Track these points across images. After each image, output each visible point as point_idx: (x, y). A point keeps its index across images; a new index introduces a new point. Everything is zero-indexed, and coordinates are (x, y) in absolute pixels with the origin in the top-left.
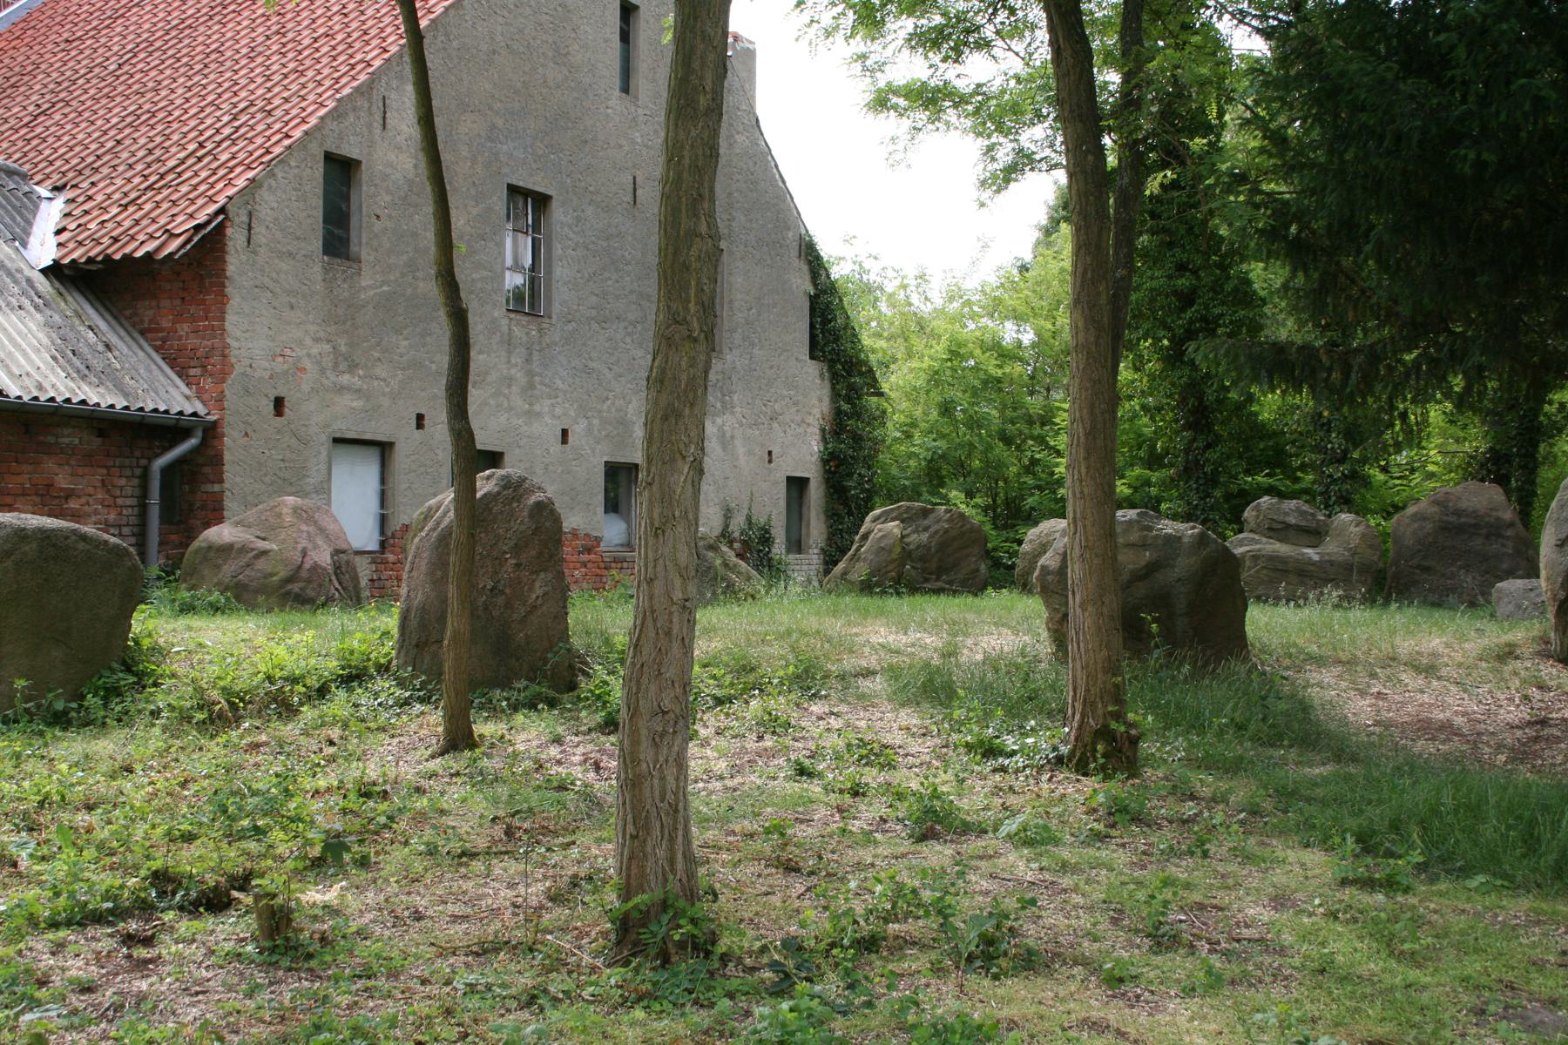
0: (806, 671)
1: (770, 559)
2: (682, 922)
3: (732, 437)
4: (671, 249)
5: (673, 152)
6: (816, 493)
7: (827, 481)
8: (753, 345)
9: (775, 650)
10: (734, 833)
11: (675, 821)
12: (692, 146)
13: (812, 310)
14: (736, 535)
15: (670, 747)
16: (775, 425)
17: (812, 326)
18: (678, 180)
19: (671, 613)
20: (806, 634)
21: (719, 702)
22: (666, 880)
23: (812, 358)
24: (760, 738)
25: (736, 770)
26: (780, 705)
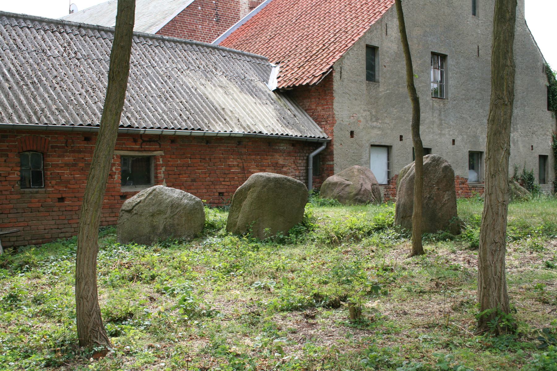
0: (549, 228)
1: (533, 186)
2: (504, 320)
3: (517, 141)
4: (496, 72)
5: (496, 35)
6: (550, 161)
8: (525, 106)
9: (537, 220)
10: (522, 288)
11: (500, 282)
12: (504, 33)
13: (548, 91)
14: (519, 177)
15: (498, 256)
16: (534, 136)
17: (548, 98)
18: (499, 46)
19: (498, 206)
20: (549, 214)
21: (515, 239)
22: (497, 304)
23: (548, 110)
24: (531, 253)
25: (522, 265)
26: (539, 241)
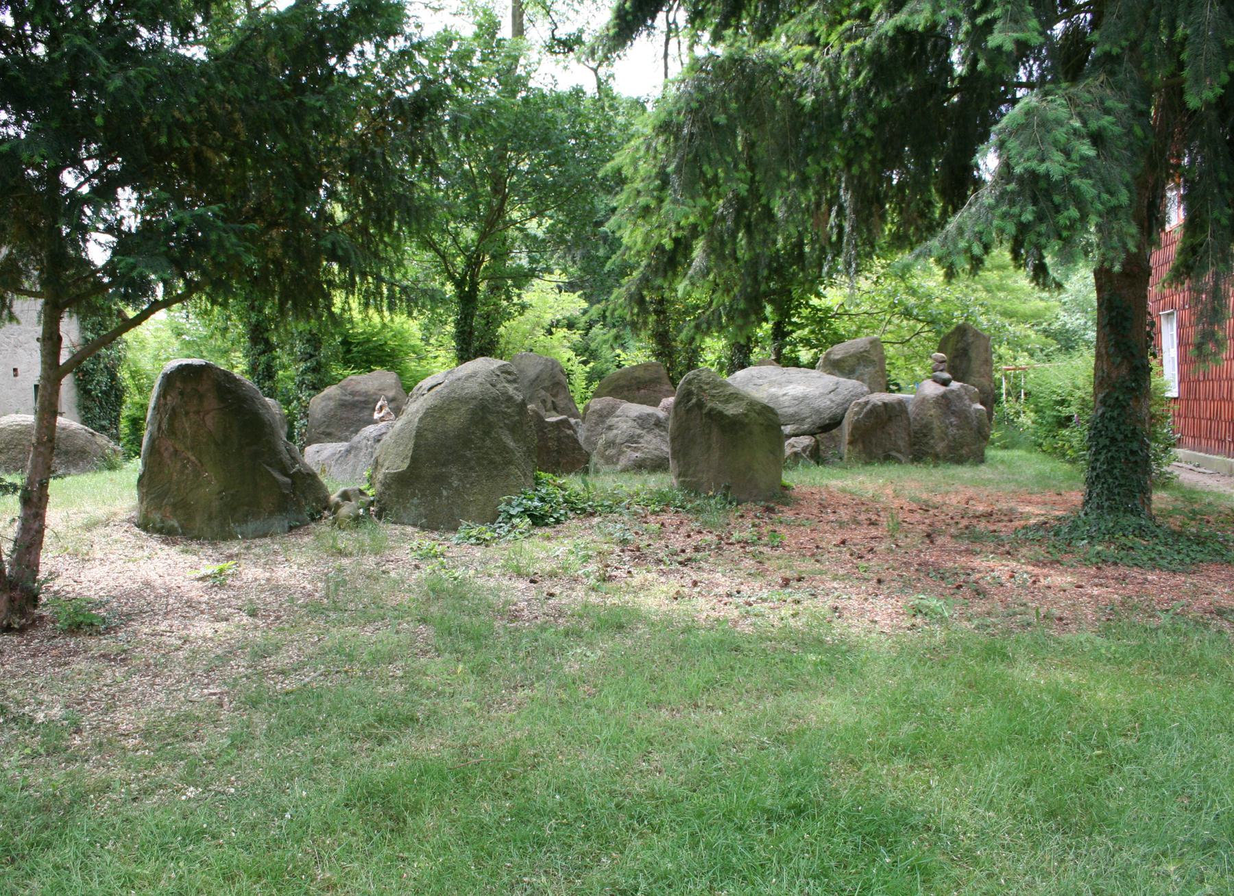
7: (78, 386)
